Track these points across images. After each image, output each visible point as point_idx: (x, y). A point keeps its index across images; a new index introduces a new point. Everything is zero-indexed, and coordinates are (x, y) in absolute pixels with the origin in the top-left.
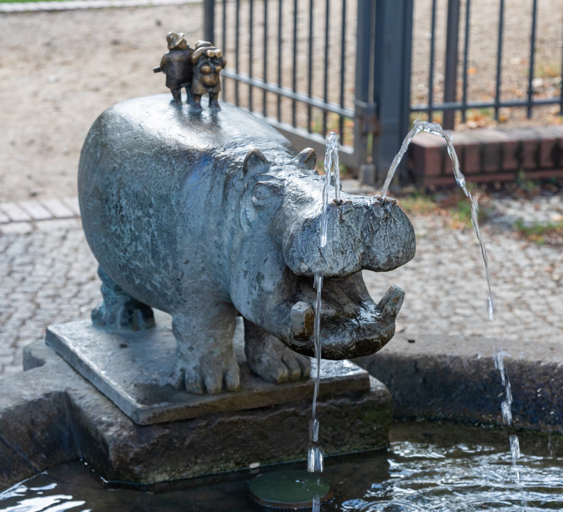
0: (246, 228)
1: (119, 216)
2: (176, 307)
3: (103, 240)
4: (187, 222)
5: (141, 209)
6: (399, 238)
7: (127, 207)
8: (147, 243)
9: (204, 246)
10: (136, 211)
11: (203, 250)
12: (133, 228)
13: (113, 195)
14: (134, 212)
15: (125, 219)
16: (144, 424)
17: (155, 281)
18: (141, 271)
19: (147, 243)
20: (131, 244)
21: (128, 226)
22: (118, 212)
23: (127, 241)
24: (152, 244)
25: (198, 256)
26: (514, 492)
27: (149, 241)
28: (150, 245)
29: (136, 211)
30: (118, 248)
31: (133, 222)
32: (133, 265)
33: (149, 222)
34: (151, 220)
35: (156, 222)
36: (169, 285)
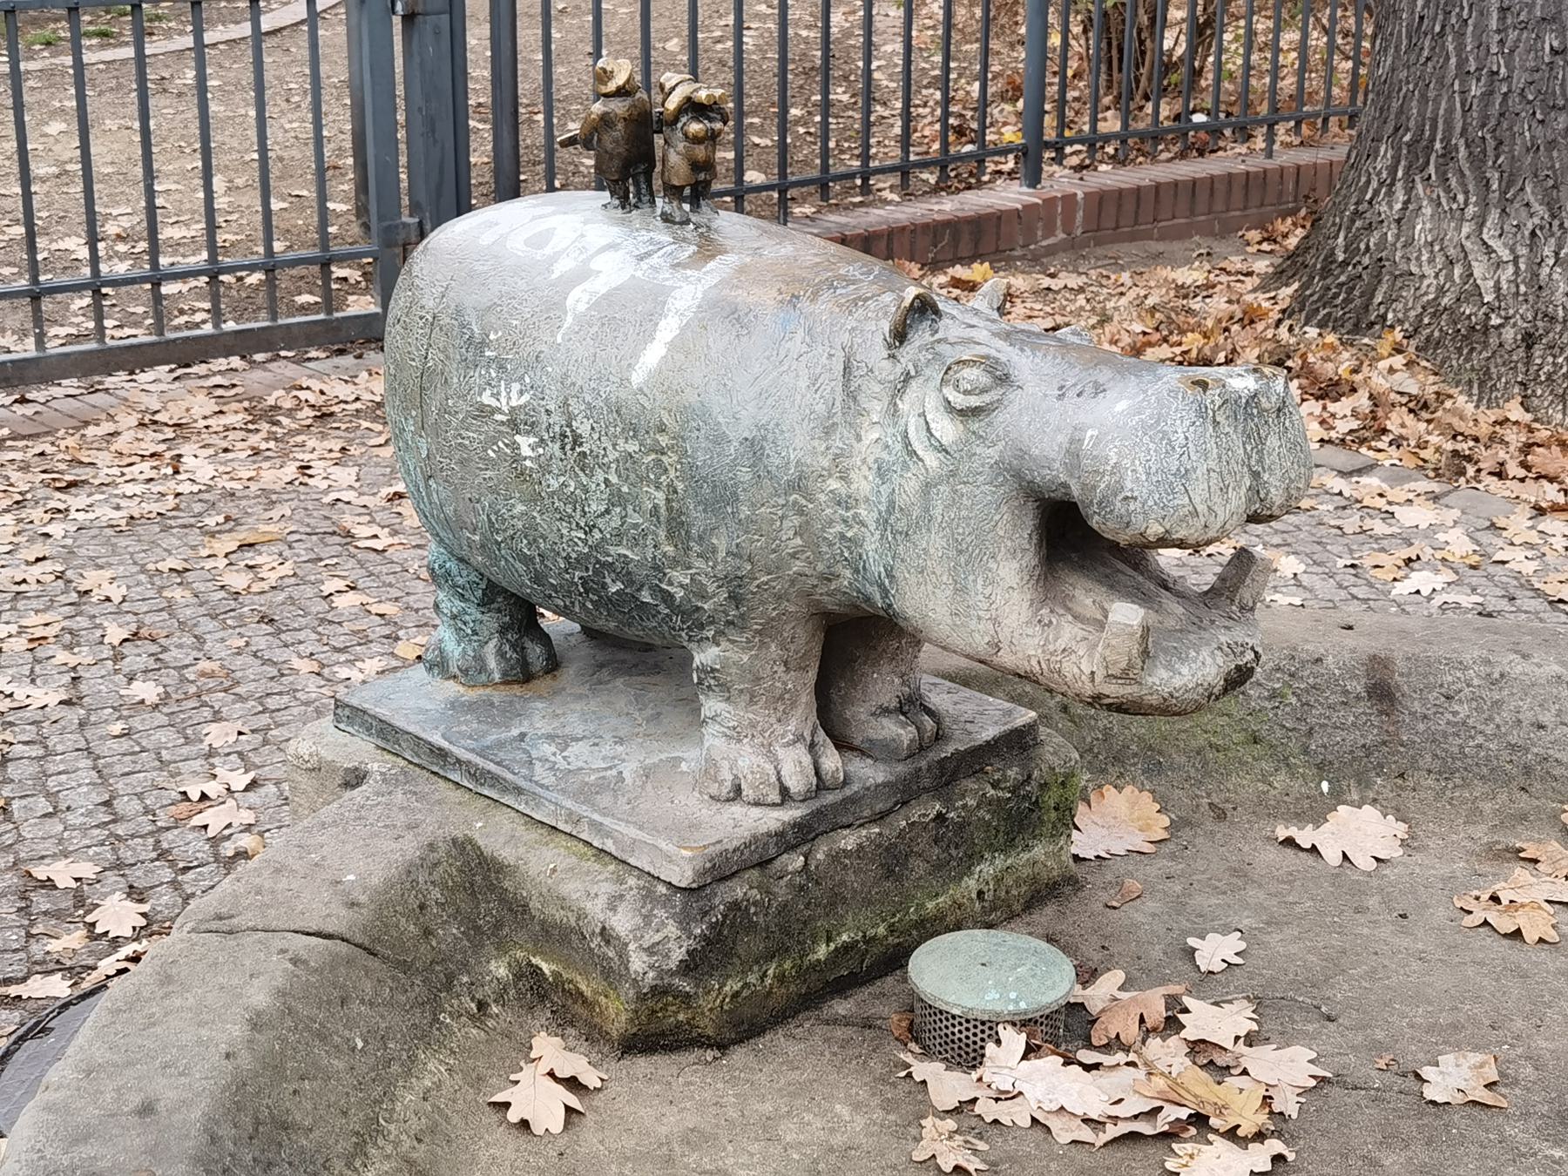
0: (931, 460)
1: (572, 457)
2: (720, 633)
3: (520, 508)
4: (762, 454)
5: (634, 436)
6: (1298, 448)
7: (596, 436)
8: (656, 507)
9: (804, 502)
10: (621, 442)
11: (801, 512)
12: (614, 479)
13: (548, 412)
14: (614, 445)
15: (588, 461)
16: (694, 885)
17: (670, 583)
18: (632, 565)
19: (656, 507)
20: (607, 511)
21: (600, 476)
22: (568, 447)
23: (595, 507)
24: (670, 509)
25: (787, 524)
26: (607, 859)
27: (662, 503)
28: (663, 511)
29: (621, 442)
30: (570, 523)
31: (614, 466)
32: (609, 555)
33: (658, 462)
34: (664, 458)
35: (679, 462)
36: (711, 588)
